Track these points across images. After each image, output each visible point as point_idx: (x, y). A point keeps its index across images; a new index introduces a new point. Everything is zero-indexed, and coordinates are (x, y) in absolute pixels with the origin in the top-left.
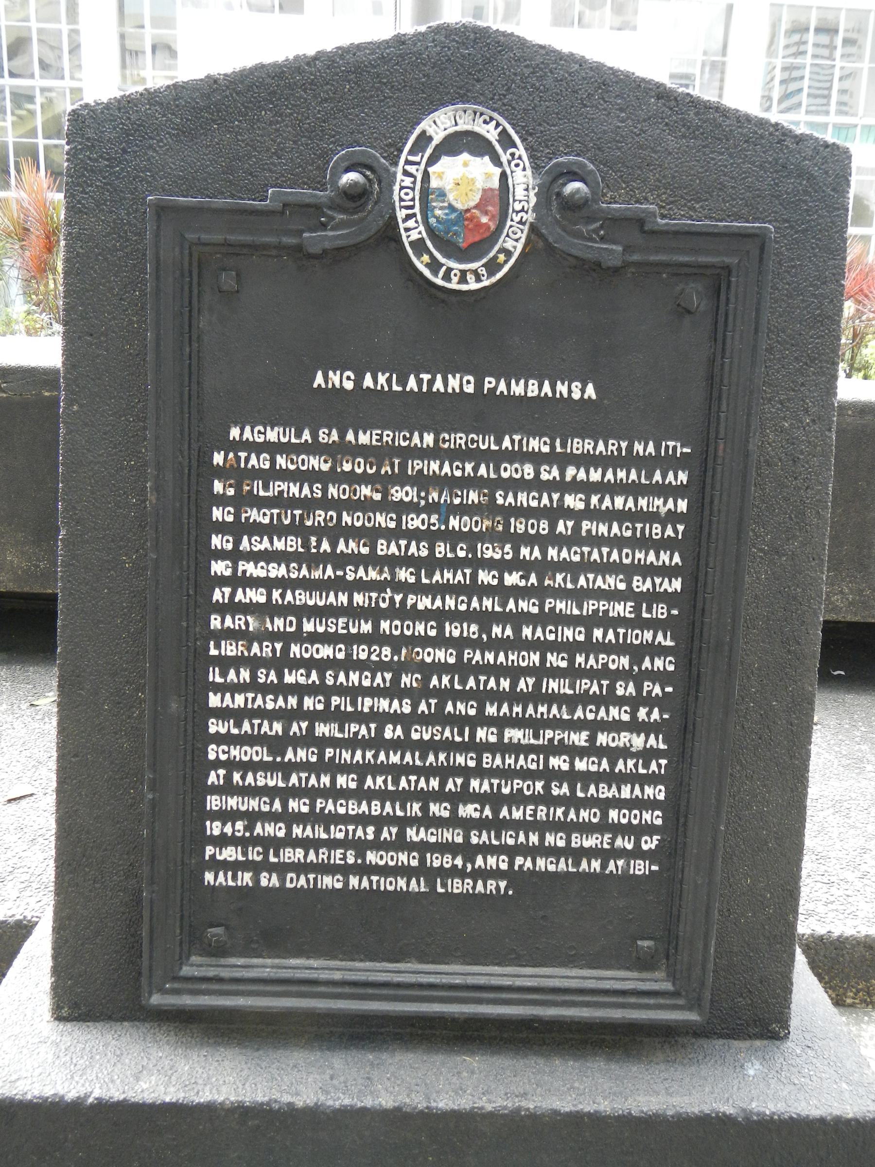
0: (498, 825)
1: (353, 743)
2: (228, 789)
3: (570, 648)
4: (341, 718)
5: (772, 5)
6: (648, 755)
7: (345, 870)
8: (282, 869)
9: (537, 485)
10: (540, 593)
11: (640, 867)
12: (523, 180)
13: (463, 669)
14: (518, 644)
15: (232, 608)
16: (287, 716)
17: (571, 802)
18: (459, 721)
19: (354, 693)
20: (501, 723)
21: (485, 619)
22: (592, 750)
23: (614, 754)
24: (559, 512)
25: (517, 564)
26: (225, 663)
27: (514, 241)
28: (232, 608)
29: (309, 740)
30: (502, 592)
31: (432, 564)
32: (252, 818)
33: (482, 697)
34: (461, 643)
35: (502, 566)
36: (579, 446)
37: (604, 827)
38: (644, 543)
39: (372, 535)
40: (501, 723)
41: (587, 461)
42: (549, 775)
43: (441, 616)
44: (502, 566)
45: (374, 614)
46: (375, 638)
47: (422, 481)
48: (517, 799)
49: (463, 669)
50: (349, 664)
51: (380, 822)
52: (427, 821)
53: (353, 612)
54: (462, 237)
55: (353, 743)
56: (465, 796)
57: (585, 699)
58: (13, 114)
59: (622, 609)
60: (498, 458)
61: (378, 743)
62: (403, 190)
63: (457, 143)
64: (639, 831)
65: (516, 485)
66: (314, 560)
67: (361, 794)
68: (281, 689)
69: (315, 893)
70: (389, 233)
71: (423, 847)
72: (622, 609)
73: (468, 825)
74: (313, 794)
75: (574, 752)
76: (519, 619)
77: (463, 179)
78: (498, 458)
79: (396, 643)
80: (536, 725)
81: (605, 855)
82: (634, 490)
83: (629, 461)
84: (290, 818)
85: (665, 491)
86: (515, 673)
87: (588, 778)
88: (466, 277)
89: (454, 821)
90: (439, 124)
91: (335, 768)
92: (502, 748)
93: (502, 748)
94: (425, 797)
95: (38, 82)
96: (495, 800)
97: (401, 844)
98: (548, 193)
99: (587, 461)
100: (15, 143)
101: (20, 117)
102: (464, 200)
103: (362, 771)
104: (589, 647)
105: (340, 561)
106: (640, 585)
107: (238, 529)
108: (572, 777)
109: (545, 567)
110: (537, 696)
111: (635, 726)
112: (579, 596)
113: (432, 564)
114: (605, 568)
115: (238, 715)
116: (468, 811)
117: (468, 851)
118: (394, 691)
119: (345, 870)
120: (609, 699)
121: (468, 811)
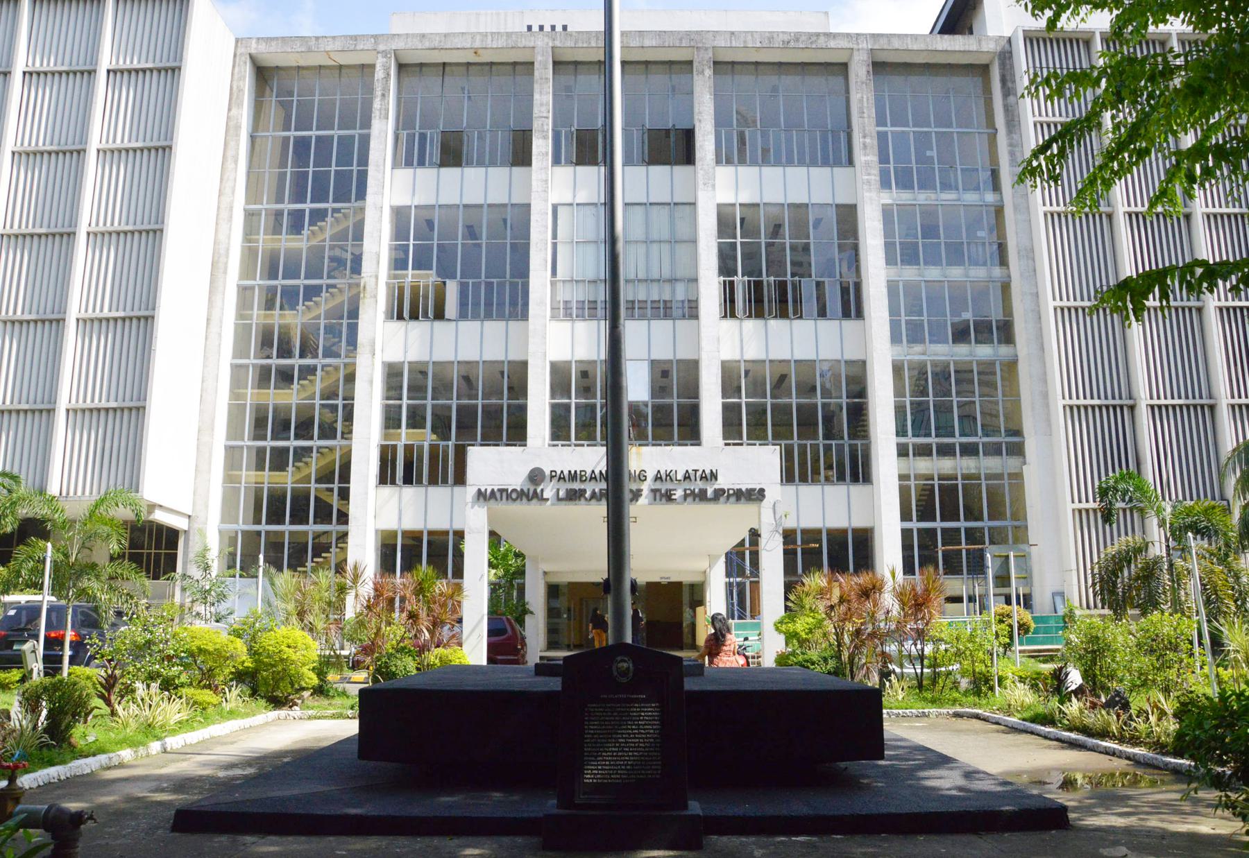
54: (624, 673)
62: (614, 668)
88: (624, 680)
101: (313, 233)
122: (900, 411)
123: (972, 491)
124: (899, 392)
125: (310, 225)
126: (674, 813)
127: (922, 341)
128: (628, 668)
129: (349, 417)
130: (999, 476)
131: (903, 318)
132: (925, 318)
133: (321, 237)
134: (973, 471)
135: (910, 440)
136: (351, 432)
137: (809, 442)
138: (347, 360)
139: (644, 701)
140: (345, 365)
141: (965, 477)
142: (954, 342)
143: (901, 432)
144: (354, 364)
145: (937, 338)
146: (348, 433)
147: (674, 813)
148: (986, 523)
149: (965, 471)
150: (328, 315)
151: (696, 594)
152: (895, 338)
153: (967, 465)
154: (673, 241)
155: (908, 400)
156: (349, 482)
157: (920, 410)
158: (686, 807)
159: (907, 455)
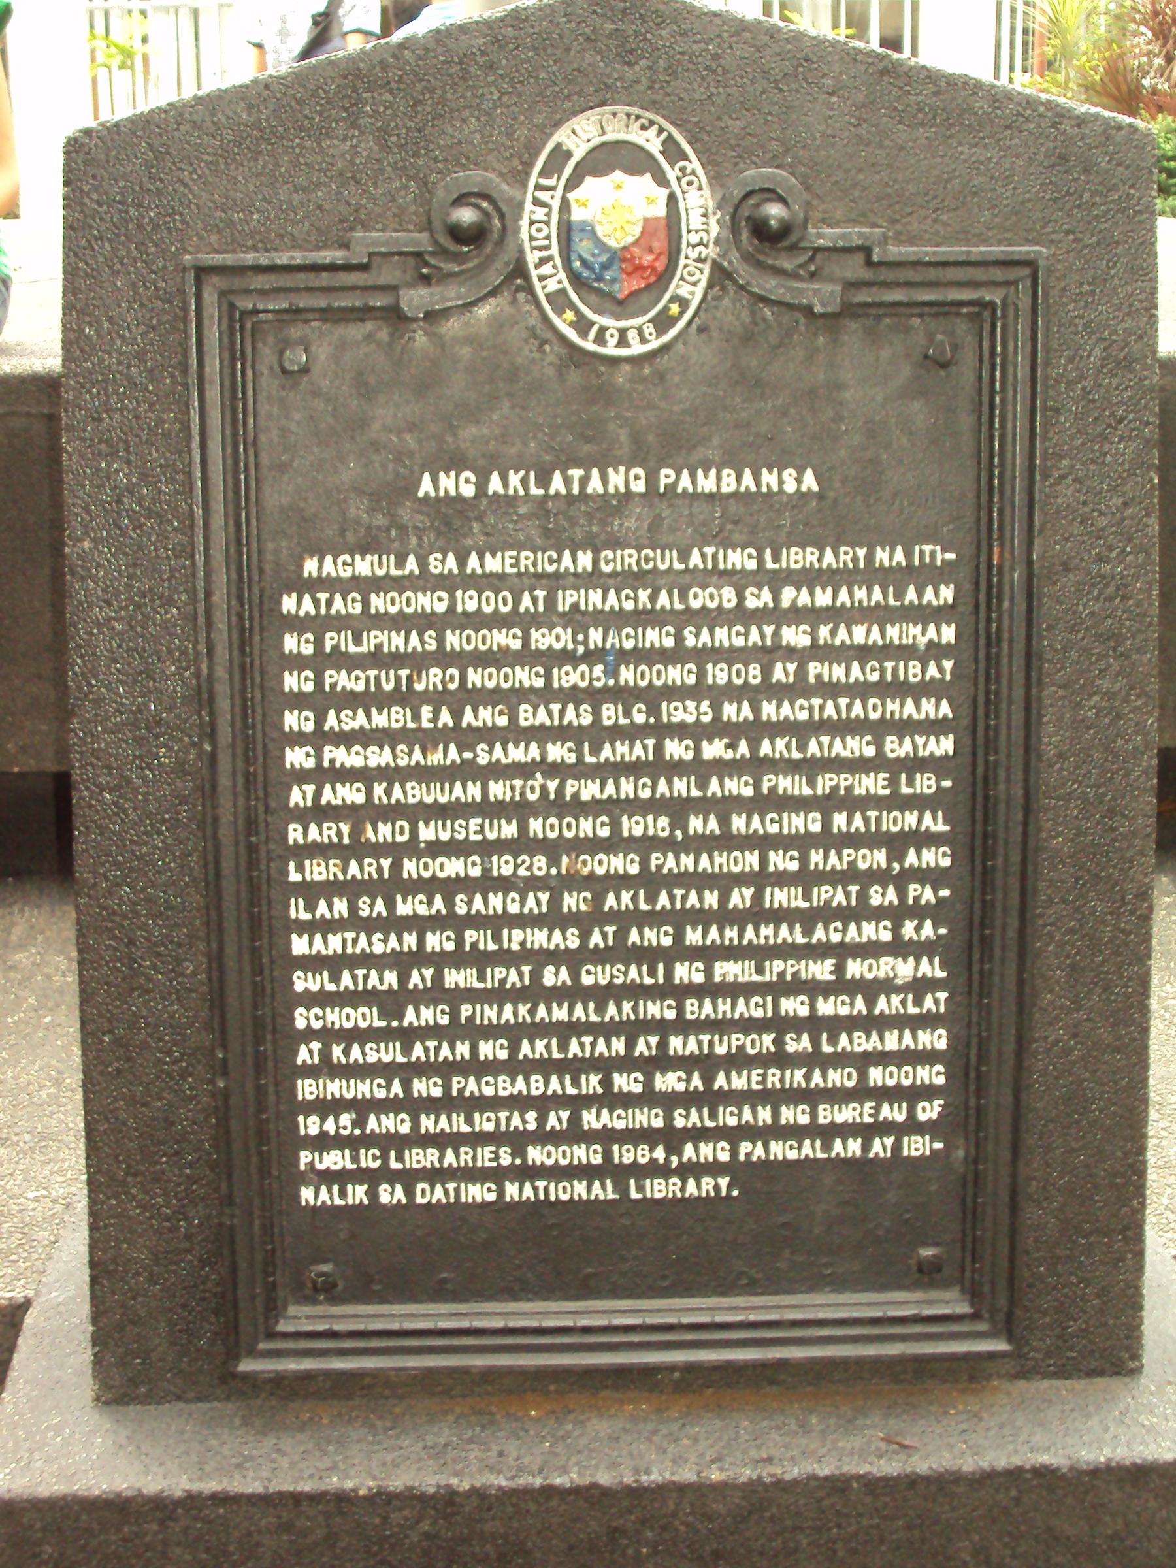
0: (711, 1099)
1: (499, 995)
2: (327, 1068)
3: (801, 843)
5: (16, 217)
6: (920, 987)
7: (497, 1175)
8: (408, 1178)
9: (742, 616)
11: (917, 1146)
12: (701, 212)
13: (650, 881)
14: (727, 841)
15: (320, 813)
16: (403, 962)
17: (814, 1060)
18: (647, 956)
19: (497, 923)
20: (708, 955)
21: (677, 809)
22: (841, 986)
23: (871, 989)
26: (312, 892)
27: (690, 285)
29: (436, 993)
30: (701, 769)
31: (598, 734)
32: (362, 1108)
33: (679, 919)
34: (646, 845)
35: (696, 732)
36: (797, 558)
37: (862, 1093)
39: (512, 698)
40: (708, 955)
41: (809, 578)
42: (780, 1025)
43: (613, 808)
44: (696, 732)
45: (520, 810)
46: (522, 845)
47: (577, 619)
48: (738, 1061)
50: (489, 884)
51: (543, 1104)
52: (611, 1099)
54: (604, 280)
55: (499, 995)
56: (662, 1061)
57: (827, 914)
59: (871, 784)
61: (535, 993)
62: (534, 231)
63: (609, 158)
66: (428, 739)
67: (514, 1067)
68: (394, 924)
69: (456, 1210)
71: (607, 1137)
72: (871, 784)
73: (670, 1101)
74: (446, 1070)
75: (815, 989)
76: (725, 806)
77: (617, 208)
78: (683, 582)
80: (760, 954)
81: (867, 1132)
83: (872, 575)
84: (414, 1106)
85: (923, 615)
86: (725, 883)
87: (836, 1025)
88: (629, 337)
89: (649, 1098)
90: (580, 134)
91: (477, 1032)
92: (710, 990)
93: (710, 990)
94: (606, 1067)
96: (706, 1064)
97: (575, 1134)
99: (809, 578)
103: (514, 1033)
104: (829, 840)
105: (467, 738)
106: (896, 748)
108: (814, 1024)
109: (757, 730)
110: (758, 914)
111: (898, 948)
112: (810, 768)
113: (598, 734)
115: (334, 964)
116: (669, 1082)
117: (672, 1138)
118: (554, 919)
119: (497, 1175)
120: (860, 912)
121: (669, 1082)
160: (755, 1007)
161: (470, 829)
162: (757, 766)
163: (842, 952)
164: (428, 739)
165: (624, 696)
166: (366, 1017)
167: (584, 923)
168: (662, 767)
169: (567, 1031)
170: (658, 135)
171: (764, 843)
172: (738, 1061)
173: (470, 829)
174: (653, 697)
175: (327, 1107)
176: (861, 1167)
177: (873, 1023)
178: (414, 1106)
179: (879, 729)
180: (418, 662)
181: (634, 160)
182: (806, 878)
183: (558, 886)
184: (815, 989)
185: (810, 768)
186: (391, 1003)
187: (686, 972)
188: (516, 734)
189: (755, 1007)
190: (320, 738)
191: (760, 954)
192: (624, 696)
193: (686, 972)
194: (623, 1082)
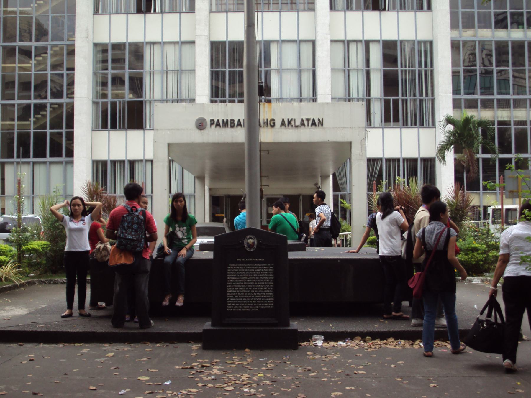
0: (257, 303)
1: (242, 295)
2: (229, 300)
3: (263, 285)
4: (241, 293)
5: (351, 143)
6: (271, 295)
7: (241, 309)
8: (235, 309)
9: (259, 269)
10: (260, 279)
11: (272, 307)
12: (256, 241)
13: (252, 287)
14: (258, 284)
15: (230, 282)
16: (235, 293)
17: (264, 300)
18: (252, 293)
19: (242, 290)
20: (257, 293)
21: (254, 282)
22: (266, 295)
23: (268, 295)
24: (261, 271)
25: (257, 276)
26: (229, 288)
27: (255, 247)
28: (230, 282)
29: (237, 295)
30: (256, 279)
31: (249, 277)
32: (232, 303)
33: (254, 290)
34: (252, 285)
35: (256, 277)
36: (263, 265)
37: (268, 303)
38: (269, 274)
39: (243, 274)
40: (257, 293)
41: (263, 266)
42: (262, 298)
43: (250, 282)
44: (256, 277)
45: (243, 282)
46: (244, 284)
47: (248, 269)
48: (259, 300)
49: (252, 287)
50: (241, 287)
51: (245, 303)
52: (250, 303)
53: (242, 282)
54: (251, 246)
55: (242, 295)
56: (253, 300)
57: (265, 290)
58: (34, 117)
59: (268, 281)
60: (255, 266)
61: (244, 295)
62: (245, 243)
63: (250, 238)
64: (271, 303)
65: (257, 269)
66: (237, 277)
67: (243, 300)
68: (234, 290)
69: (239, 311)
70: (244, 246)
71: (249, 306)
72: (268, 281)
73: (254, 303)
74: (238, 301)
75: (264, 295)
76: (258, 282)
77: (250, 241)
78: (255, 266)
79: (246, 285)
80: (260, 293)
81: (268, 306)
82: (268, 269)
83: (268, 266)
84: (235, 303)
85: (271, 269)
86: (258, 287)
87: (266, 298)
88: (251, 250)
89: (252, 303)
90: (248, 237)
91: (240, 298)
92: (257, 295)
93: (257, 295)
94: (249, 301)
95: (50, 101)
96: (256, 301)
97: (247, 305)
98: (258, 242)
99: (263, 266)
100: (34, 133)
101: (37, 119)
102: (250, 243)
103: (243, 298)
104: (265, 284)
105: (240, 277)
106: (270, 278)
107: (230, 274)
108: (264, 298)
109: (260, 277)
110: (260, 290)
111: (270, 292)
112: (264, 279)
113: (249, 277)
114: (266, 277)
115: (230, 293)
116: (254, 302)
117: (254, 306)
118: (246, 290)
119: (241, 309)
120: (267, 290)
121: (254, 302)
122: (455, 75)
123: (504, 133)
124: (455, 63)
125: (34, 114)
126: (282, 328)
127: (473, 27)
128: (254, 243)
129: (71, 84)
130: (524, 123)
131: (460, 10)
132: (476, 10)
133: (43, 10)
134: (506, 119)
135: (463, 96)
136: (73, 93)
137: (391, 98)
138: (68, 43)
139: (260, 262)
140: (68, 45)
141: (500, 123)
142: (495, 28)
143: (456, 91)
144: (74, 45)
145: (487, 26)
146: (71, 94)
147: (282, 328)
148: (513, 155)
149: (500, 119)
150: (54, 10)
151: (312, 197)
152: (454, 25)
153: (503, 115)
154: (179, 72)
155: (461, 69)
156: (73, 128)
157: (470, 74)
158: (288, 325)
159: (460, 107)
160: (260, 296)
161: (240, 283)
162: (260, 279)
163: (266, 293)
164: (237, 277)
165: (251, 274)
166: (232, 297)
167: (248, 290)
168: (253, 279)
169: (246, 298)
170: (239, 120)
171: (260, 285)
172: (259, 300)
173: (240, 283)
174: (253, 274)
175: (229, 303)
176: (268, 308)
177: (268, 298)
178: (235, 303)
179: (268, 277)
180: (237, 272)
181: (252, 239)
182: (263, 287)
183: (246, 287)
184: (264, 295)
185: (264, 279)
186: (234, 296)
187: (255, 294)
188: (243, 277)
189: (260, 296)
190: (230, 277)
191: (260, 293)
192: (251, 274)
193: (255, 294)
194: (251, 302)
